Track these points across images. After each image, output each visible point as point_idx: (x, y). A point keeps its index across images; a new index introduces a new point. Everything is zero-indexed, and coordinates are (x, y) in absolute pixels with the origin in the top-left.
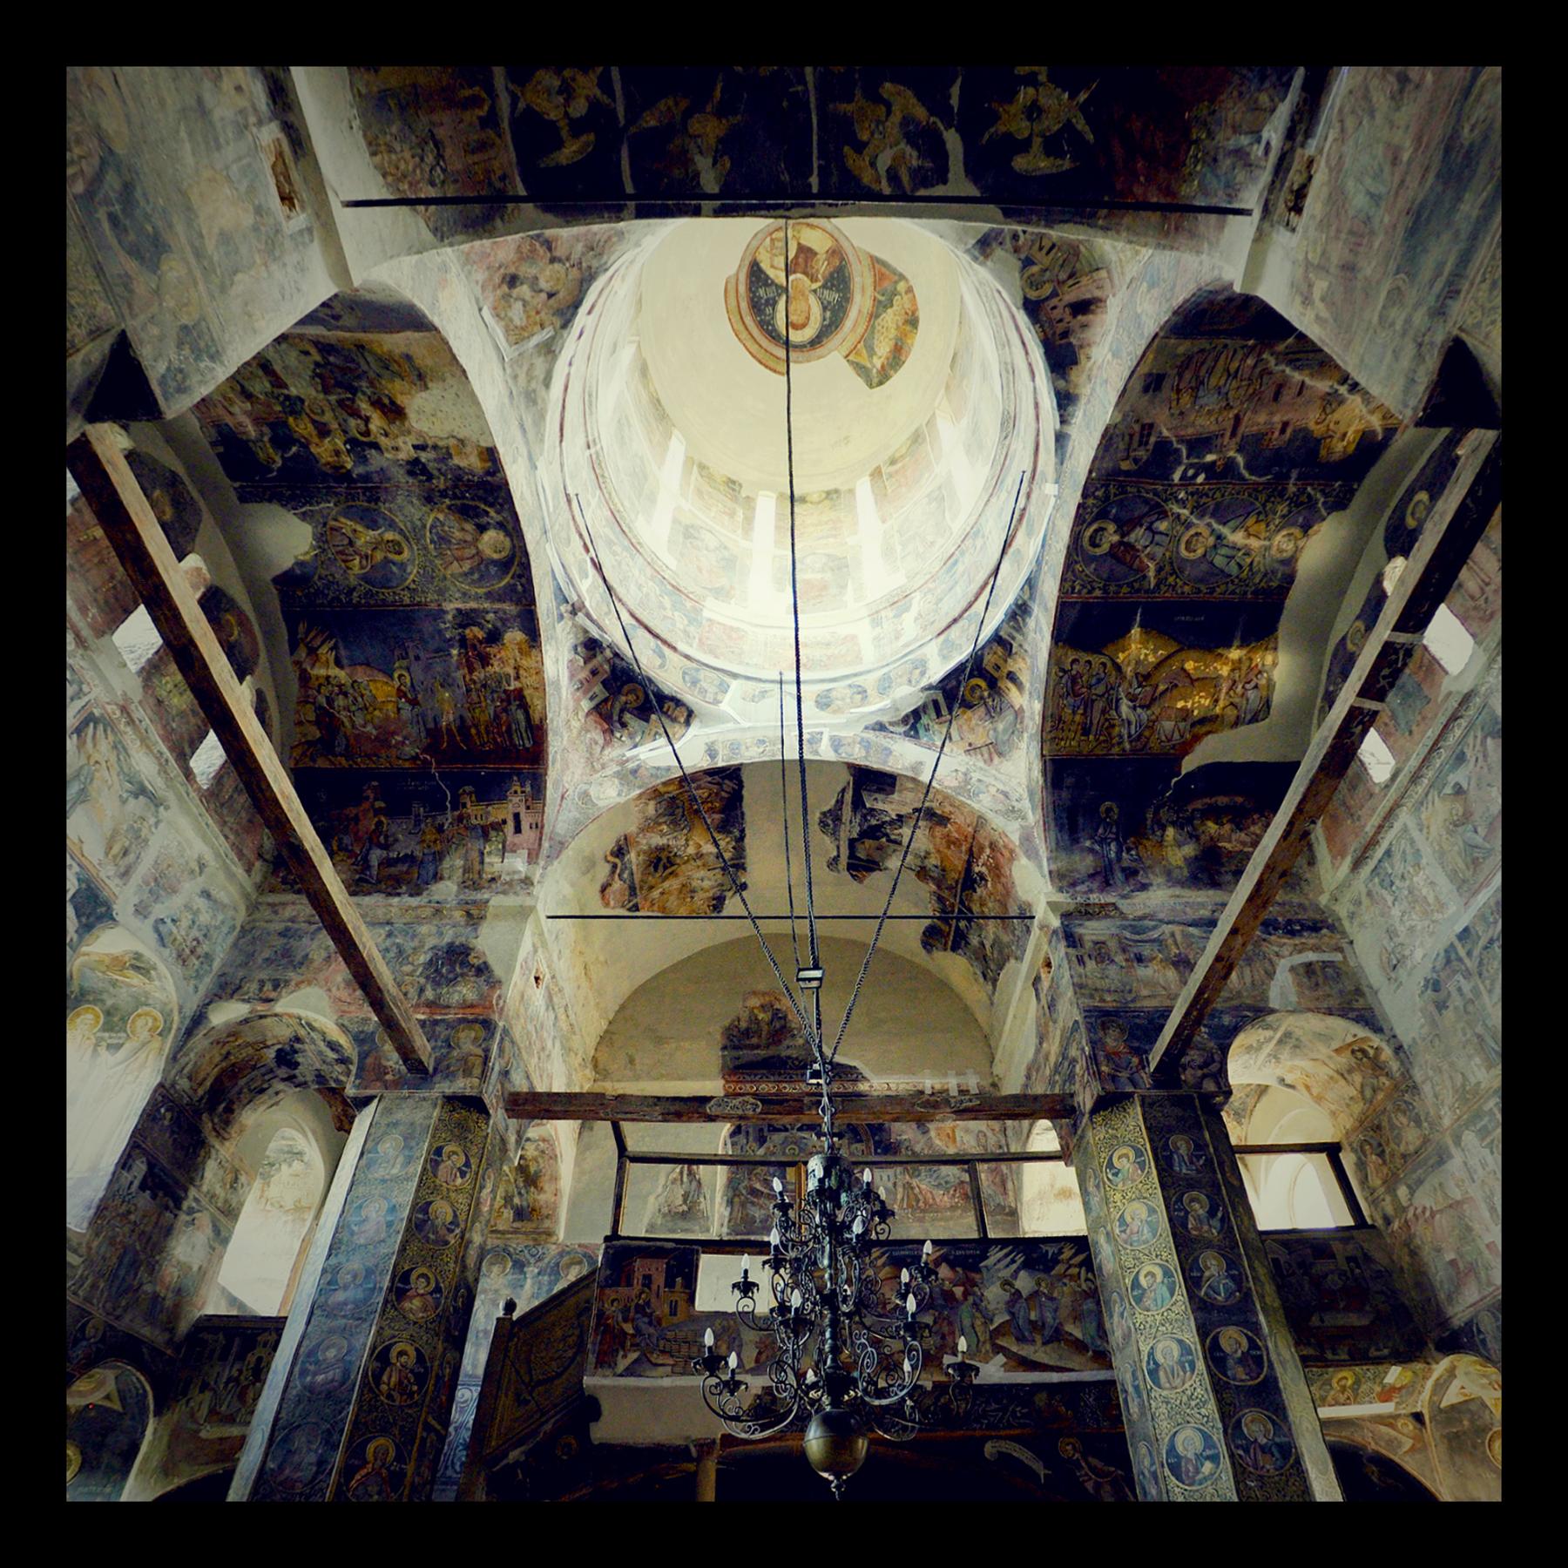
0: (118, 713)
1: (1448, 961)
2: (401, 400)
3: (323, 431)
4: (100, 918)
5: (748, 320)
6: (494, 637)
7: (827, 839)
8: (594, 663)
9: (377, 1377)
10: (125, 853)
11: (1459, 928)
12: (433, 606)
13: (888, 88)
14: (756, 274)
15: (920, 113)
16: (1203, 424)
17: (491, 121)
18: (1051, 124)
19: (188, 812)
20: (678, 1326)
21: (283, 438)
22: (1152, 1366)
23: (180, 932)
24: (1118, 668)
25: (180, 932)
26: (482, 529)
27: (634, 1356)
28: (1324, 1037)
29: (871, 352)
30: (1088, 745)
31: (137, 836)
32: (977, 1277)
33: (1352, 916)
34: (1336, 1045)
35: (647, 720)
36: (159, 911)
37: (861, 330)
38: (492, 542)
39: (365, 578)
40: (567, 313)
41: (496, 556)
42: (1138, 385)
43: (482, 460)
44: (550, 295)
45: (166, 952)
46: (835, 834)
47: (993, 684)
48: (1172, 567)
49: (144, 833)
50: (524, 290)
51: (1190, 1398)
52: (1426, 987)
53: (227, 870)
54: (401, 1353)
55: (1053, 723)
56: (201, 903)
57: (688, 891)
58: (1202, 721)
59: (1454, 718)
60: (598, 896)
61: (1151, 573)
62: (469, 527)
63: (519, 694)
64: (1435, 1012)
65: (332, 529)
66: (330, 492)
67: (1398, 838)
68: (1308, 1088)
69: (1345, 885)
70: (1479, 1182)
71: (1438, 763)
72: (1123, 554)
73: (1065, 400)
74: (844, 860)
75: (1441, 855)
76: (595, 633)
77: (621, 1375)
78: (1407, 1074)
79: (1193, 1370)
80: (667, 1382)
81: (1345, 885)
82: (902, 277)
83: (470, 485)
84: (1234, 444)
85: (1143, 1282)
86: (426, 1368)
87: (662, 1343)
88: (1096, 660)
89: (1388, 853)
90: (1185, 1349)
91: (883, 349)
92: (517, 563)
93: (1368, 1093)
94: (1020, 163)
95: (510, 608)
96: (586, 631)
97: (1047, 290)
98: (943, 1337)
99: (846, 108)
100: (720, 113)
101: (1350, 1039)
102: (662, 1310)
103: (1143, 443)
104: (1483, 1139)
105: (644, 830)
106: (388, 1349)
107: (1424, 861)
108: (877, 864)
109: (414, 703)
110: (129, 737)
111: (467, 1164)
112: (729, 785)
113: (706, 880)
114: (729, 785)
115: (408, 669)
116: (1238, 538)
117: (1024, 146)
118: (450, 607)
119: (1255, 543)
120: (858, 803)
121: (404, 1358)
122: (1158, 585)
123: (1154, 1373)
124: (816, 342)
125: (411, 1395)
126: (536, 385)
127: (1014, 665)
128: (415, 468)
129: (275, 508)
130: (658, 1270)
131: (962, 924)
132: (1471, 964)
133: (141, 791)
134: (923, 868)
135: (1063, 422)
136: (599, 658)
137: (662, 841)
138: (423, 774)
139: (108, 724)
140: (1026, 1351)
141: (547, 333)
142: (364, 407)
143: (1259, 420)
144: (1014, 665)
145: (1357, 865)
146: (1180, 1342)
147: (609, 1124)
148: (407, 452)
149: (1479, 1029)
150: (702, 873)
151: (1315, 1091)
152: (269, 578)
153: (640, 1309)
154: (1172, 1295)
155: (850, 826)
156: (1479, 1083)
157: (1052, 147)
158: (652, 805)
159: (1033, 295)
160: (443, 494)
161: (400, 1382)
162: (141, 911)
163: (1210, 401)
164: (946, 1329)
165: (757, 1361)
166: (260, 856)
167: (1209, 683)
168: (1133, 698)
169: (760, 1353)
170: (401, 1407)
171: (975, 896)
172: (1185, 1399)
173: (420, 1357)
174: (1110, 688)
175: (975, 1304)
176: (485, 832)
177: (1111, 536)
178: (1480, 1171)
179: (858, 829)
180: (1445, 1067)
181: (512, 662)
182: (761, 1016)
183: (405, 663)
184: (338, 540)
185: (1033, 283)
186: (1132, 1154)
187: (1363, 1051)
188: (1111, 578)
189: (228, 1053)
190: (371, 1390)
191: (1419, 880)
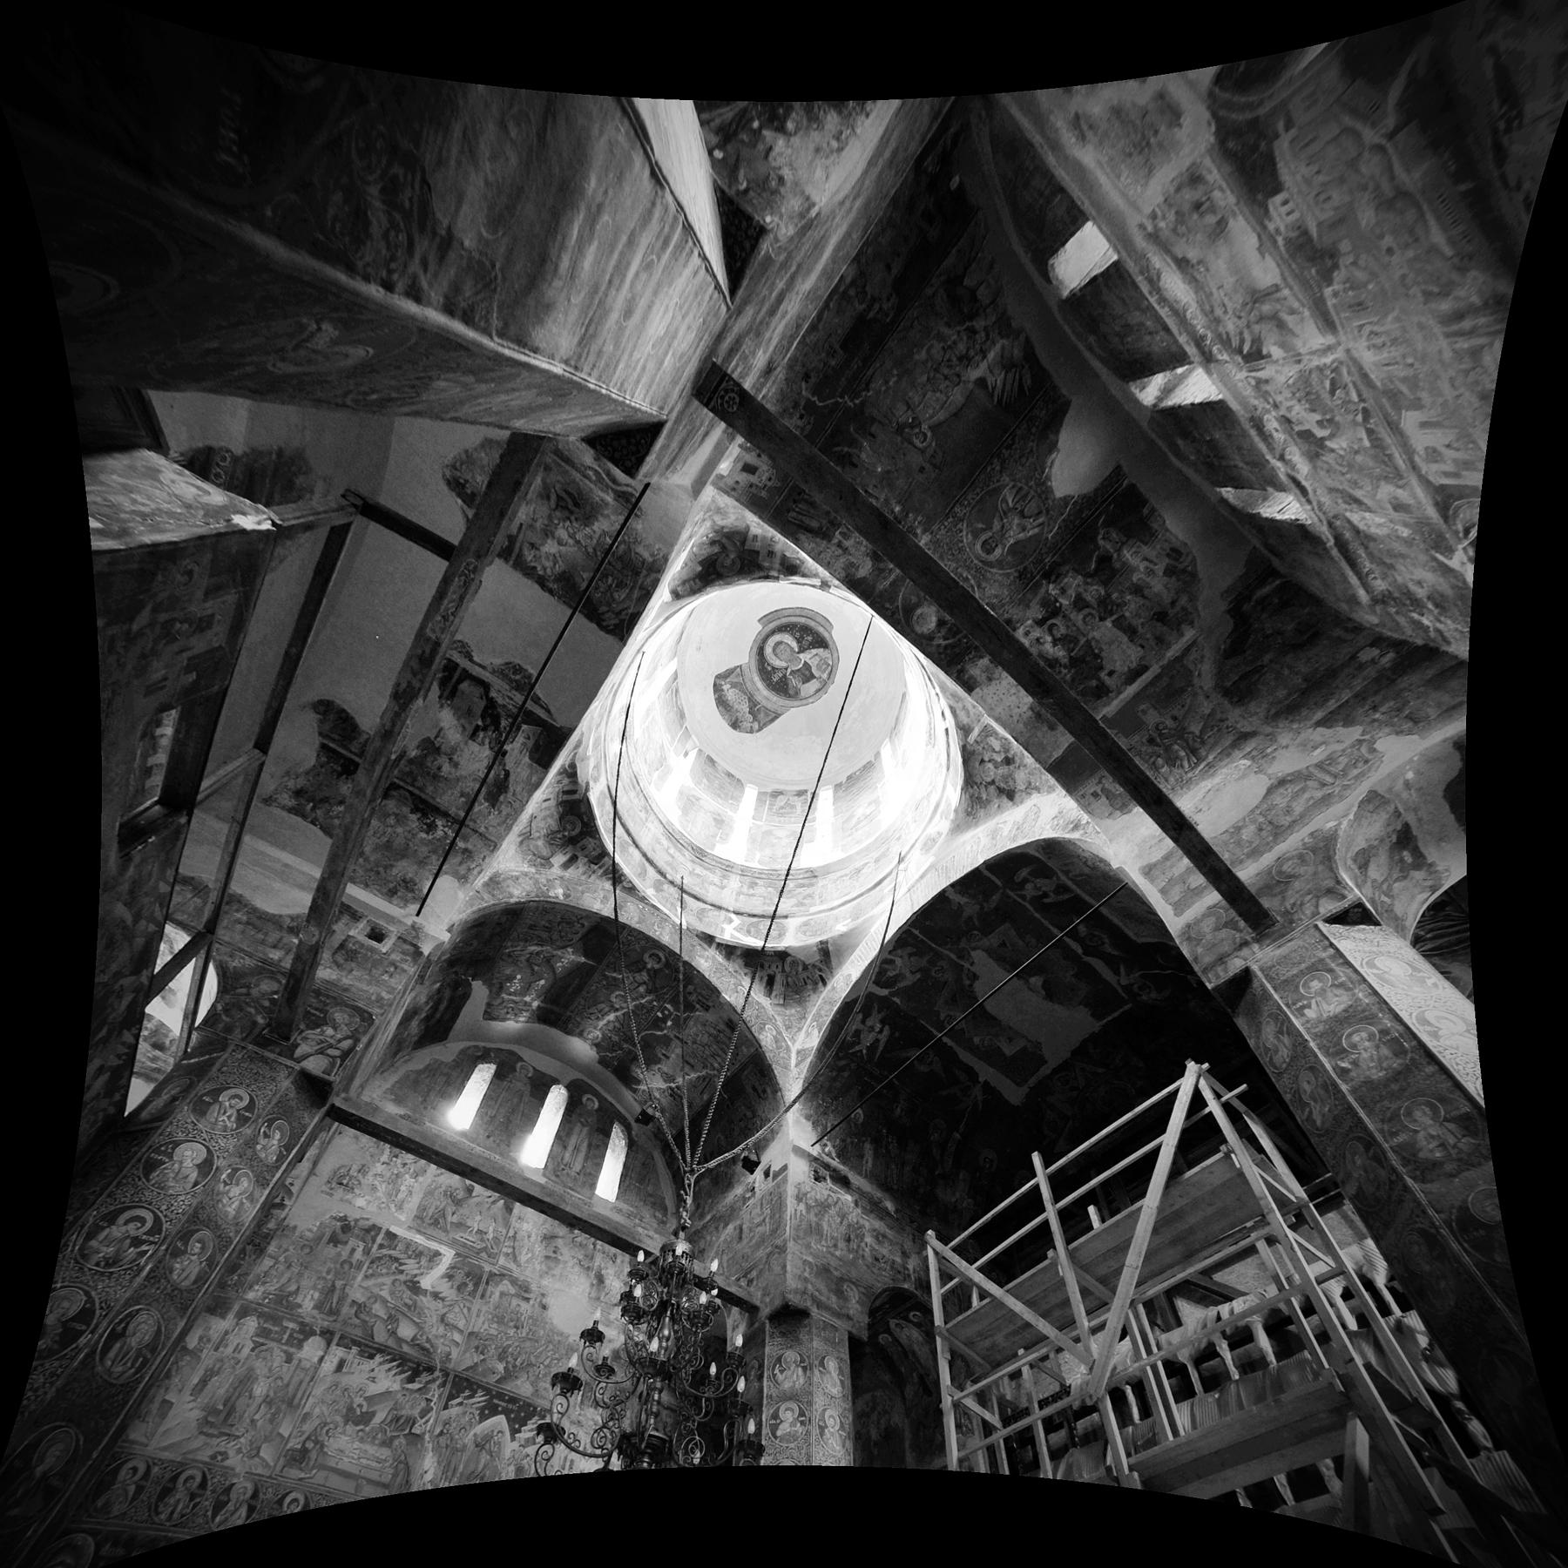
0: (1215, 350)
1: (368, 1231)
3: (1080, 603)
5: (803, 620)
7: (498, 661)
8: (777, 561)
10: (1197, 206)
11: (394, 1229)
12: (935, 528)
13: (918, 976)
14: (821, 643)
15: (901, 985)
16: (692, 1029)
24: (564, 947)
29: (734, 685)
35: (701, 563)
37: (749, 684)
39: (998, 491)
41: (919, 611)
43: (971, 677)
44: (982, 761)
46: (501, 672)
48: (614, 985)
50: (999, 758)
58: (501, 988)
65: (1040, 513)
70: (217, 1354)
72: (637, 966)
73: (729, 950)
74: (463, 663)
82: (760, 729)
91: (731, 694)
95: (883, 585)
96: (804, 575)
97: (787, 968)
99: (926, 959)
100: (970, 918)
103: (699, 1002)
104: (257, 1335)
107: (421, 1179)
109: (900, 429)
110: (1200, 324)
114: (612, 621)
115: (923, 451)
122: (606, 978)
124: (761, 652)
129: (1088, 488)
135: (719, 945)
136: (777, 566)
137: (597, 526)
143: (676, 1051)
149: (339, 1284)
152: (1076, 402)
155: (503, 693)
156: (300, 1306)
159: (789, 960)
167: (526, 990)
168: (538, 954)
171: (406, 810)
178: (230, 1349)
179: (500, 701)
180: (295, 1269)
181: (852, 551)
183: (930, 451)
184: (1031, 507)
185: (795, 963)
191: (408, 1180)
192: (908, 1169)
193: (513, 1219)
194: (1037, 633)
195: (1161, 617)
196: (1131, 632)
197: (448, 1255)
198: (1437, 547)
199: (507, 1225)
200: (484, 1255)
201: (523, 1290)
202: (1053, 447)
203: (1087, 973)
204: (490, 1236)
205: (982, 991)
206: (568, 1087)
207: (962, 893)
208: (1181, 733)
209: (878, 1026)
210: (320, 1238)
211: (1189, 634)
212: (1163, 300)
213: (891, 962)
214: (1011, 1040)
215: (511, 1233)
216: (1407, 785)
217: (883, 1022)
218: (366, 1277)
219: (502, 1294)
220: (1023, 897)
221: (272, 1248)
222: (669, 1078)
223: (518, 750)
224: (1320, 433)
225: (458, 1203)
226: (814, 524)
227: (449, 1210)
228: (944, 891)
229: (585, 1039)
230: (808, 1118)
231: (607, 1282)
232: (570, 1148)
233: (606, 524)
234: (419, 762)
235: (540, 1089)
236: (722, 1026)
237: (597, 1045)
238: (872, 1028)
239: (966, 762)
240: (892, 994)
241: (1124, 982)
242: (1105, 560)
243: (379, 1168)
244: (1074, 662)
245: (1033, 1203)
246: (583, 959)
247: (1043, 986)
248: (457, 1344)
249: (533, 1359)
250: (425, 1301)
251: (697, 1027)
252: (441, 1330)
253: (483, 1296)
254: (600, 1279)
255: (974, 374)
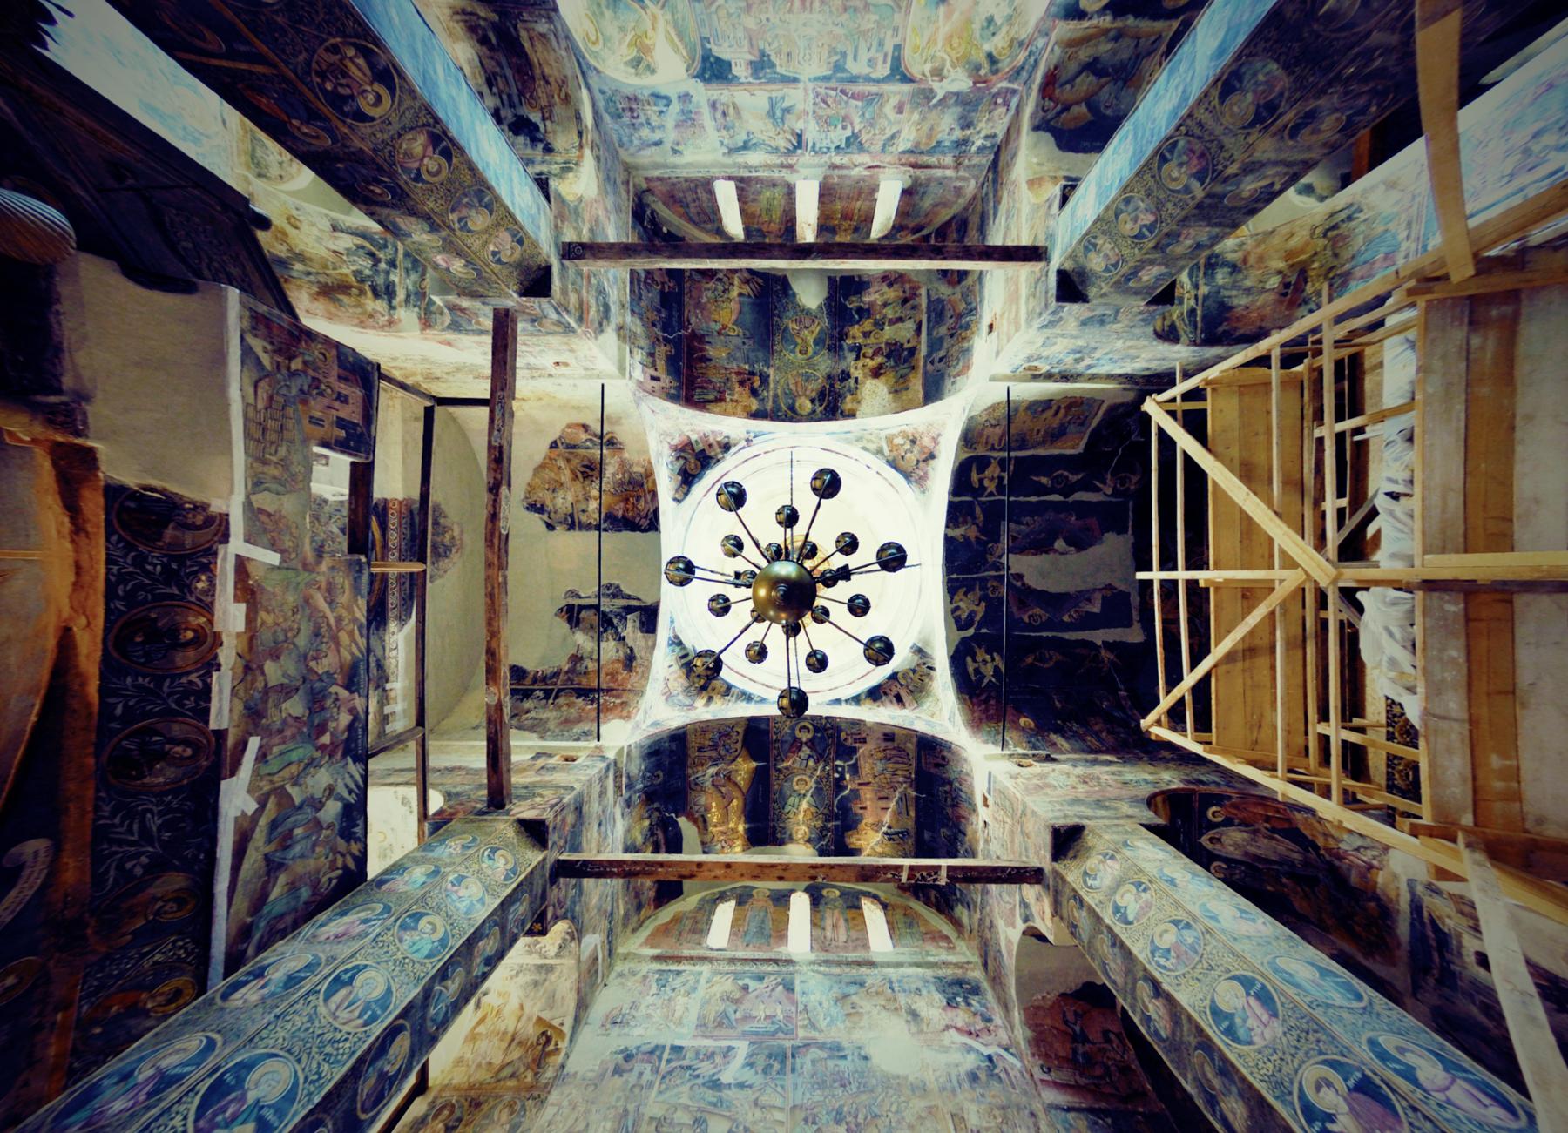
1: (652, 1052)
2: (883, 378)
3: (866, 335)
4: (703, 70)
6: (754, 393)
9: (366, 53)
10: (724, 114)
11: (678, 1043)
13: (983, 604)
15: (978, 618)
16: (866, 768)
17: (993, 449)
18: (983, 670)
19: (713, 165)
20: (299, 422)
21: (864, 313)
22: (346, 977)
23: (651, 112)
24: (734, 760)
25: (651, 112)
26: (813, 401)
27: (266, 360)
28: (551, 1001)
30: (693, 753)
31: (726, 128)
32: (338, 756)
33: (621, 975)
34: (546, 1015)
36: (676, 107)
38: (805, 405)
39: (786, 328)
40: (893, 464)
42: (887, 730)
45: (646, 93)
47: (703, 688)
48: (788, 774)
49: (724, 132)
50: (908, 446)
51: (333, 1042)
52: (622, 1052)
53: (665, 166)
54: (379, 99)
55: (703, 728)
56: (656, 136)
57: (556, 487)
58: (705, 821)
59: (776, 961)
60: (582, 421)
61: (785, 764)
62: (814, 394)
63: (720, 399)
64: (610, 1072)
66: (834, 327)
67: (692, 973)
68: (482, 1020)
69: (640, 958)
71: (747, 968)
73: (856, 700)
74: (576, 602)
75: (706, 1003)
76: (733, 450)
77: (242, 339)
78: (548, 1088)
79: (366, 1024)
80: (234, 393)
81: (640, 958)
83: (836, 400)
84: (855, 786)
85: (423, 923)
86: (347, 115)
87: (281, 400)
88: (739, 745)
89: (678, 973)
90: (384, 1001)
92: (791, 415)
93: (507, 1072)
94: (969, 659)
95: (769, 406)
98: (280, 731)
101: (556, 1023)
102: (317, 407)
103: (855, 741)
105: (623, 463)
106: (392, 90)
108: (577, 624)
109: (719, 333)
110: (774, 159)
111: (499, 261)
112: (645, 523)
113: (562, 502)
114: (645, 523)
116: (804, 805)
117: (974, 661)
118: (771, 372)
119: (801, 817)
120: (629, 609)
121: (371, 98)
123: (338, 983)
125: (323, 75)
126: (864, 443)
127: (717, 698)
128: (845, 376)
129: (825, 295)
130: (353, 412)
131: (541, 694)
132: (664, 1067)
133: (746, 146)
134: (581, 658)
138: (683, 324)
139: (790, 152)
140: (259, 836)
141: (886, 452)
142: (879, 359)
143: (868, 795)
144: (717, 698)
145: (658, 958)
146: (389, 991)
147: (487, 396)
148: (855, 373)
149: (631, 1107)
150: (570, 498)
151: (482, 1029)
153: (316, 383)
154: (428, 957)
157: (977, 671)
158: (641, 470)
160: (832, 386)
161: (345, 74)
162: (685, 97)
163: (879, 766)
164: (288, 733)
165: (261, 511)
166: (648, 190)
167: (725, 819)
168: (717, 774)
169: (269, 515)
170: (314, 51)
171: (573, 699)
172: (327, 1037)
173: (361, 117)
174: (722, 758)
175: (313, 760)
176: (651, 355)
177: (805, 737)
182: (447, 536)
184: (807, 322)
185: (905, 675)
186: (510, 866)
187: (548, 1040)
188: (782, 742)
189: (548, 83)
190: (357, 36)
192: (1104, 735)
193: (798, 996)
194: (860, 363)
195: (905, 301)
196: (900, 320)
197: (742, 1048)
198: (929, 99)
199: (794, 1003)
200: (780, 1035)
201: (836, 1050)
202: (794, 295)
203: (1083, 509)
204: (781, 1017)
205: (1032, 581)
206: (806, 890)
207: (957, 526)
208: (960, 316)
209: (988, 657)
210: (603, 1075)
211: (923, 292)
212: (756, 170)
213: (957, 608)
214: (1089, 600)
215: (801, 1007)
216: (1039, 164)
217: (989, 652)
218: (660, 1092)
219: (813, 1062)
220: (991, 494)
221: (554, 1097)
222: (877, 825)
223: (631, 630)
224: (848, 133)
225: (737, 1002)
226: (711, 397)
227: (730, 1011)
228: (949, 541)
229: (796, 841)
230: (986, 742)
231: (923, 1014)
232: (829, 928)
233: (611, 470)
234: (572, 671)
235: (782, 899)
236: (883, 745)
237: (809, 841)
238: (985, 662)
239: (896, 468)
240: (978, 628)
241: (1109, 491)
242: (860, 310)
243: (650, 1000)
244: (888, 356)
245: (1169, 588)
246: (754, 764)
247: (1069, 544)
248: (782, 1123)
249: (876, 1110)
250: (727, 1094)
251: (869, 760)
252: (758, 1114)
253: (793, 1070)
254: (914, 1015)
255: (735, 293)
